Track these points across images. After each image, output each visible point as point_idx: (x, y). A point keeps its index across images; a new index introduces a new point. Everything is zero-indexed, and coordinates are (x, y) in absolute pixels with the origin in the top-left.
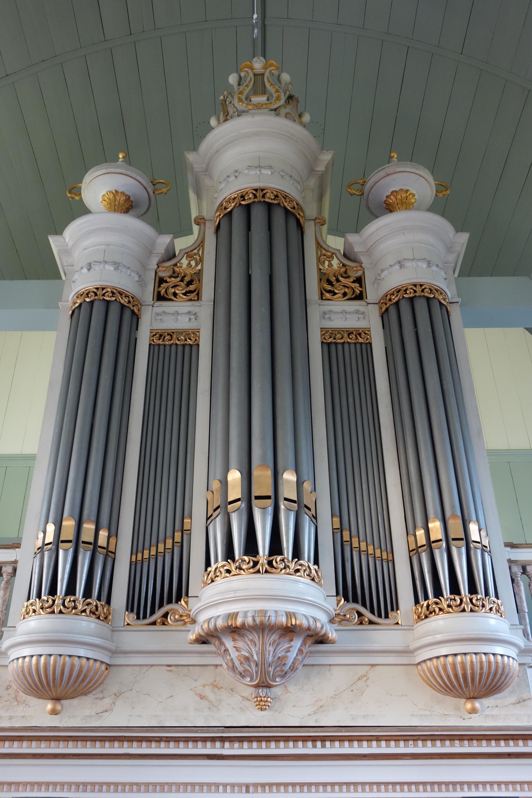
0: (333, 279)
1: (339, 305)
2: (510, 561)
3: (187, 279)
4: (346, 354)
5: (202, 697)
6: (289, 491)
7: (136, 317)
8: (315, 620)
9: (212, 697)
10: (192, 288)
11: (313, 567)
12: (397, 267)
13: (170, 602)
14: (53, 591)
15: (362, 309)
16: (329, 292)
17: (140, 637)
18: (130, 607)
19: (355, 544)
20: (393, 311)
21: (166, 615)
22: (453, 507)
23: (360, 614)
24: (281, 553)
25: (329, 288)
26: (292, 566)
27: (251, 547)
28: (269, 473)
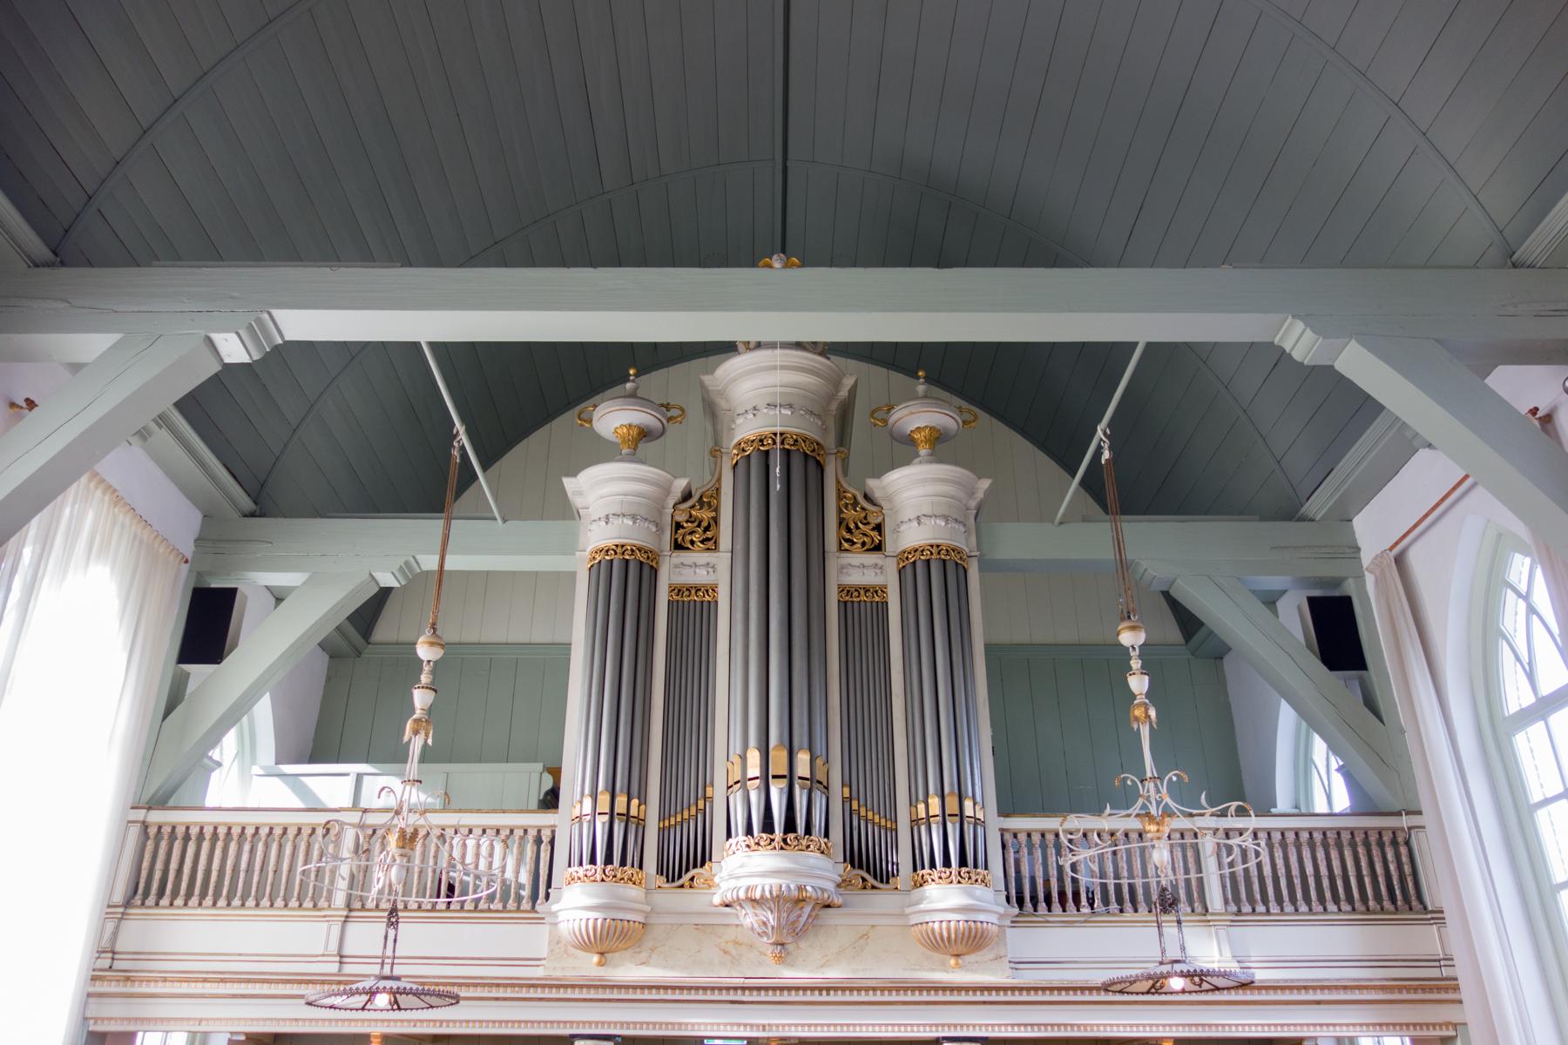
0: (852, 526)
1: (857, 558)
2: (1003, 831)
3: (705, 524)
4: (863, 610)
5: (725, 952)
6: (803, 769)
7: (654, 572)
8: (823, 890)
9: (734, 952)
10: (709, 534)
11: (823, 840)
12: (915, 523)
13: (695, 866)
14: (593, 861)
15: (880, 562)
16: (847, 540)
17: (671, 898)
18: (660, 871)
19: (863, 813)
20: (909, 570)
21: (692, 879)
22: (952, 784)
23: (864, 880)
24: (795, 831)
25: (848, 536)
26: (804, 842)
27: (768, 827)
28: (785, 753)
